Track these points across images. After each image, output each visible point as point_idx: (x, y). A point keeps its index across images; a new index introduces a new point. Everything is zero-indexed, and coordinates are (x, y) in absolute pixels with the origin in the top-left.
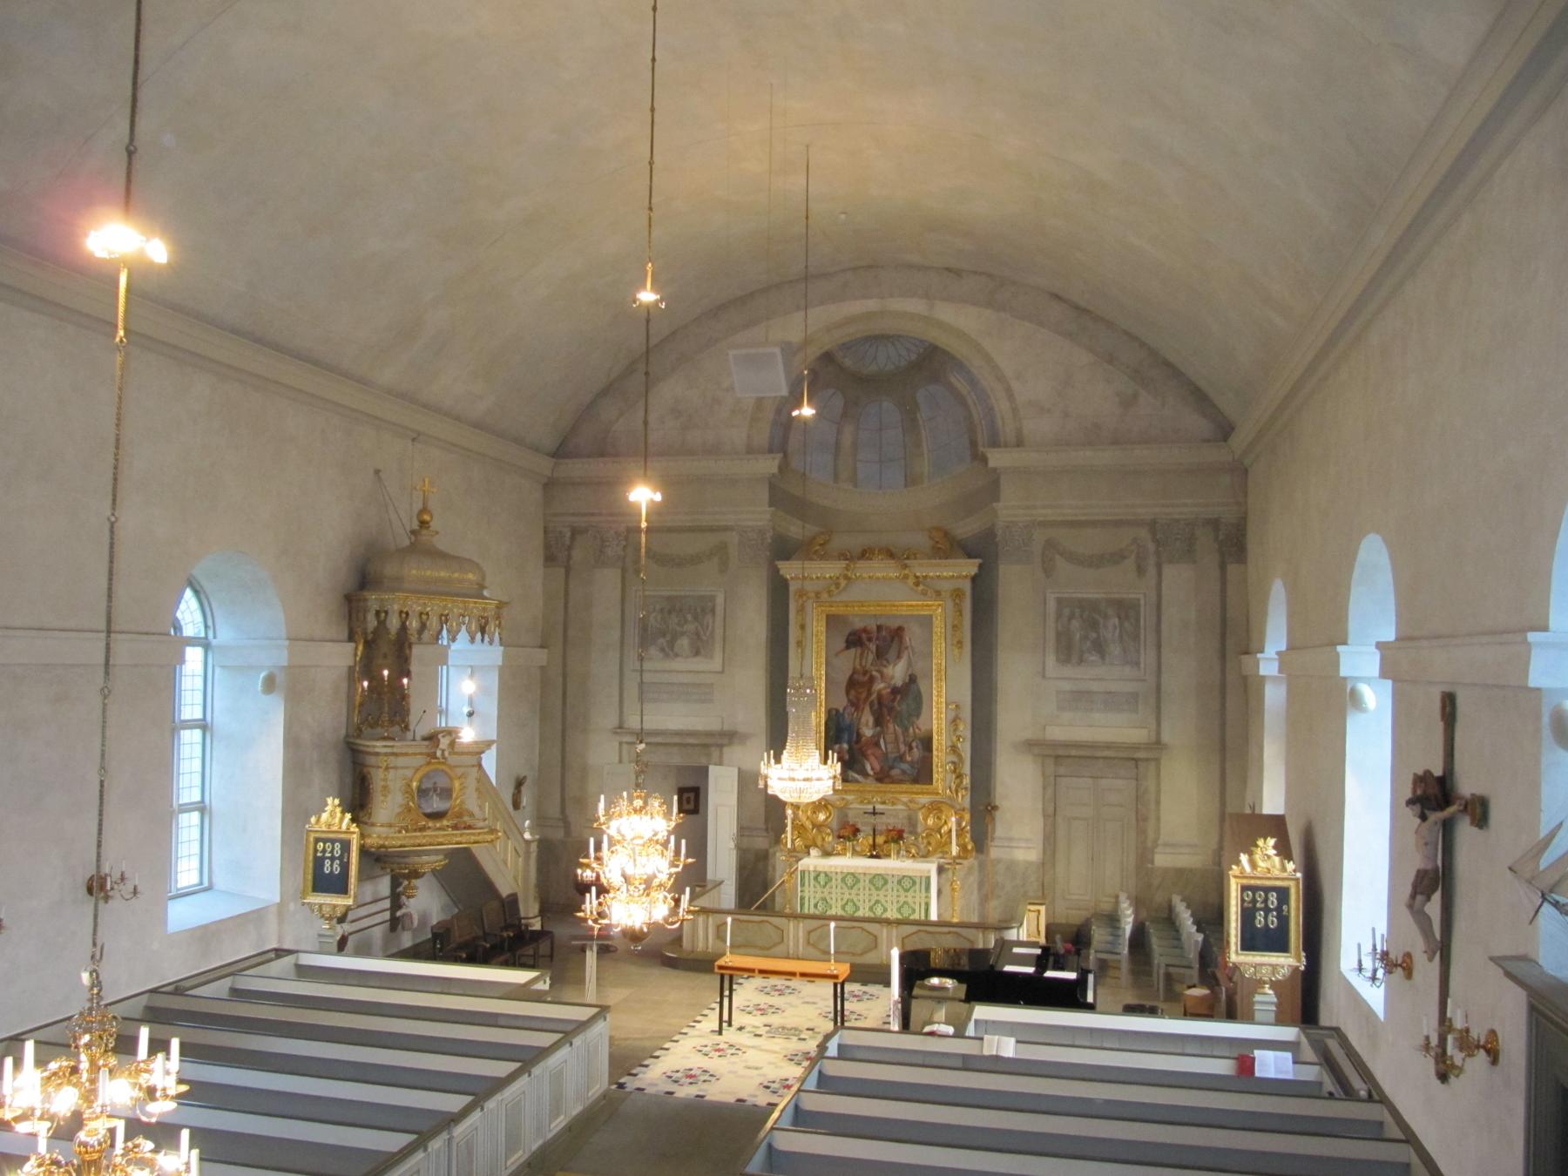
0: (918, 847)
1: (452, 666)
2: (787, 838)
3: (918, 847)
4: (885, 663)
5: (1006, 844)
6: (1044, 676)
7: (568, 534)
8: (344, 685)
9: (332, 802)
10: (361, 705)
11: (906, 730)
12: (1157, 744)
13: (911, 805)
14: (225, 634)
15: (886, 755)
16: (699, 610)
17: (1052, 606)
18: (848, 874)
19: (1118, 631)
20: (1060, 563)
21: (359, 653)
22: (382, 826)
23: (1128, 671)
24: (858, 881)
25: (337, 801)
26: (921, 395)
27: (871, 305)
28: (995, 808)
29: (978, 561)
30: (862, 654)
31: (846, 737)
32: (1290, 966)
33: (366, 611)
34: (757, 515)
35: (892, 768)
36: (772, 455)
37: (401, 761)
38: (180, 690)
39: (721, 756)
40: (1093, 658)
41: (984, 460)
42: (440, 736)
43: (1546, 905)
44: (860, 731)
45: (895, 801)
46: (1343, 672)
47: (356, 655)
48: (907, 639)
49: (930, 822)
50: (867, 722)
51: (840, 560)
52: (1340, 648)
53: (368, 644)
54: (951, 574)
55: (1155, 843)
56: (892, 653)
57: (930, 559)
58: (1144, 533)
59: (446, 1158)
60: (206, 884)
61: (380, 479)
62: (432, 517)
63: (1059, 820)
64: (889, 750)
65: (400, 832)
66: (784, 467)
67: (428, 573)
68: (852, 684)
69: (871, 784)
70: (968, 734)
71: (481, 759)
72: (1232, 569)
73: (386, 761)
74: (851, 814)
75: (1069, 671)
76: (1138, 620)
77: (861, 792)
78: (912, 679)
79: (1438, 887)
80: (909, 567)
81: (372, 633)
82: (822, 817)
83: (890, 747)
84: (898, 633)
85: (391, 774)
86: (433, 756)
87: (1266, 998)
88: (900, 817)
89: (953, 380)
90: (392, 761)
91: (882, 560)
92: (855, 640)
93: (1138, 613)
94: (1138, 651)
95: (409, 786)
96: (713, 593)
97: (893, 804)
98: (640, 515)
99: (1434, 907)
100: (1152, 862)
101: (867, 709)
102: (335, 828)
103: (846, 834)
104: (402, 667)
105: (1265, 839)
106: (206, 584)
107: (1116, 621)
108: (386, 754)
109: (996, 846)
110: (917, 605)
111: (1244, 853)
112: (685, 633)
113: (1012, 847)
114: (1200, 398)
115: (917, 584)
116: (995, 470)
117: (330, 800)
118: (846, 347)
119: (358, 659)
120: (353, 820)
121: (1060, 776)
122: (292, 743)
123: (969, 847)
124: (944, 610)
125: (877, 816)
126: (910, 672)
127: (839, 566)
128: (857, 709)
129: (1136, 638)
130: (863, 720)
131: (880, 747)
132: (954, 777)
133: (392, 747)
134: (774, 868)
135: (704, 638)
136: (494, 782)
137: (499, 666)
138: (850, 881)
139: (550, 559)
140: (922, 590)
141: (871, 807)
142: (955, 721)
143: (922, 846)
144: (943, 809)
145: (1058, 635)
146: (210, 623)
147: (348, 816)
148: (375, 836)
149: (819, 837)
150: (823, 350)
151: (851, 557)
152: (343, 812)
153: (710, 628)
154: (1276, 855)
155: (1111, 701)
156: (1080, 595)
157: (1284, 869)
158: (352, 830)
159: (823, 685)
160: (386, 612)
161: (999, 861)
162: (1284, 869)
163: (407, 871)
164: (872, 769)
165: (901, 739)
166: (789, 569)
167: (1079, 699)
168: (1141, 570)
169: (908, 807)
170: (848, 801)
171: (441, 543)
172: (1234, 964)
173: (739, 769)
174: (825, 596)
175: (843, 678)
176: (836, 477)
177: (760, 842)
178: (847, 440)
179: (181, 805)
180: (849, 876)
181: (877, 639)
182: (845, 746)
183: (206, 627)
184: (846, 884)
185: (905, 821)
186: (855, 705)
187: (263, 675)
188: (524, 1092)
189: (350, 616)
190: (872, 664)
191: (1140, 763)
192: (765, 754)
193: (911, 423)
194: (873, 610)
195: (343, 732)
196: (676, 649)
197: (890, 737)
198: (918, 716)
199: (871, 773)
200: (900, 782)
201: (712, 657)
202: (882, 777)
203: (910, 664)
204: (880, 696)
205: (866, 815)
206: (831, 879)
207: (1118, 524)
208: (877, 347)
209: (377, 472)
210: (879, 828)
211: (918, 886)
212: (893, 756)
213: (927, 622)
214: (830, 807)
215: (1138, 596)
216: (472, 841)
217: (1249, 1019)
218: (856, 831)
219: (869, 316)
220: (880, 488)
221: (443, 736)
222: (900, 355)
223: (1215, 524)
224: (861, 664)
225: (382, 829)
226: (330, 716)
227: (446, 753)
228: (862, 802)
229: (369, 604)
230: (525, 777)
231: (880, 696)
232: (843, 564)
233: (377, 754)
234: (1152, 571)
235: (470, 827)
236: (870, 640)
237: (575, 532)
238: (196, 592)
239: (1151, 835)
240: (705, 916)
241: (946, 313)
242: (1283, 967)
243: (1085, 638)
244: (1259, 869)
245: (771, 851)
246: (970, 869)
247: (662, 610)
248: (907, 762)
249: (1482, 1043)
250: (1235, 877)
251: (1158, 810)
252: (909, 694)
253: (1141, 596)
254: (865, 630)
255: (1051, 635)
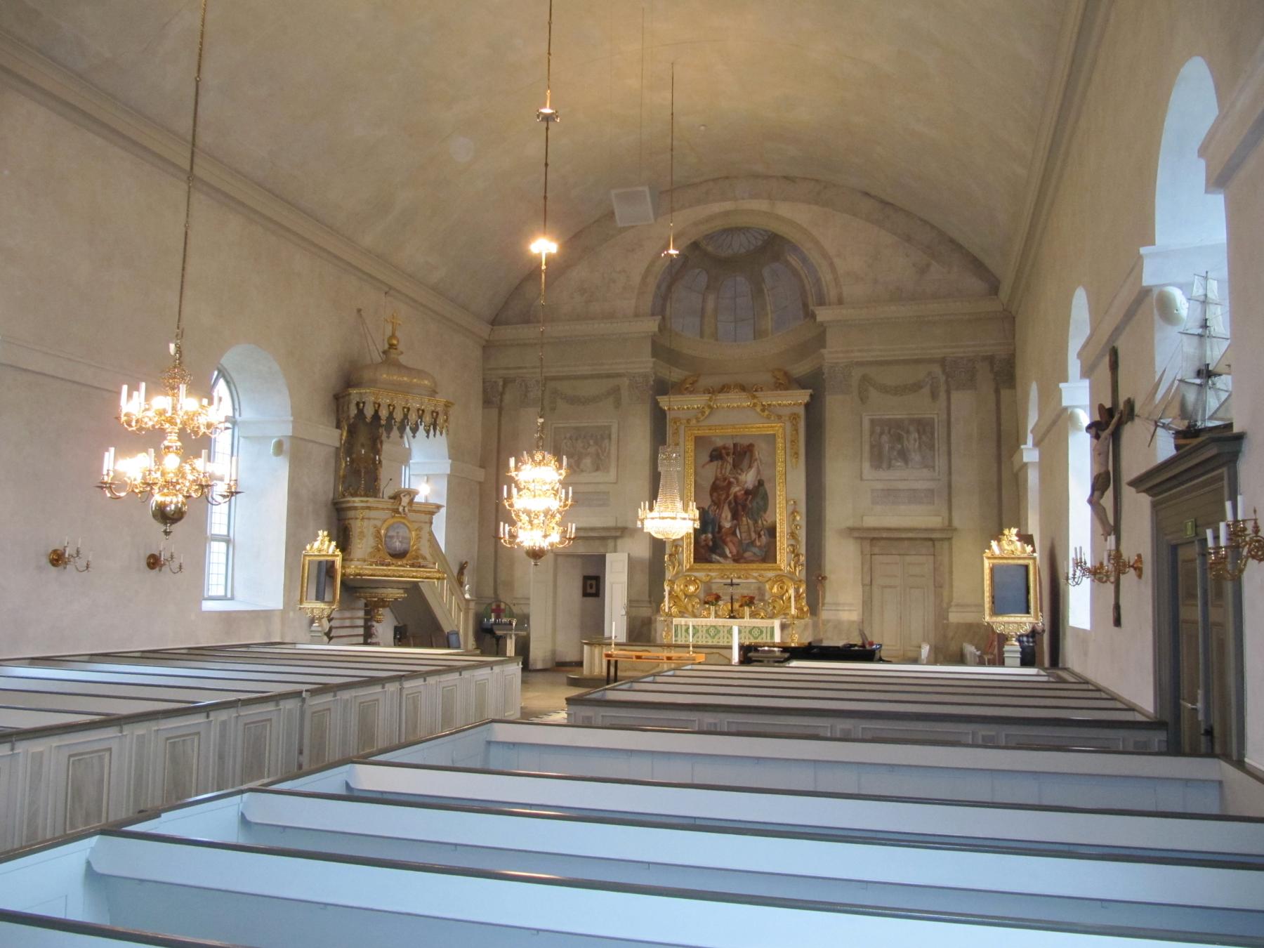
0: (766, 611)
1: (413, 475)
2: (665, 605)
3: (766, 611)
4: (739, 471)
5: (833, 608)
6: (862, 479)
7: (501, 383)
8: (333, 461)
9: (322, 534)
10: (345, 477)
11: (756, 522)
12: (950, 528)
13: (760, 578)
14: (247, 414)
15: (740, 542)
16: (599, 437)
17: (866, 425)
18: (711, 626)
19: (917, 443)
20: (873, 393)
21: (344, 438)
22: (358, 560)
23: (925, 473)
24: (719, 632)
25: (326, 533)
26: (766, 272)
27: (728, 206)
28: (824, 578)
29: (810, 391)
30: (722, 465)
31: (710, 529)
32: (1030, 623)
33: (349, 403)
34: (644, 364)
35: (745, 551)
36: (654, 317)
37: (373, 514)
38: (215, 452)
39: (615, 546)
40: (899, 464)
41: (813, 316)
42: (402, 495)
43: (1158, 429)
44: (721, 524)
45: (748, 576)
46: (1065, 403)
47: (341, 439)
48: (757, 453)
49: (775, 590)
50: (726, 517)
51: (704, 393)
52: (1062, 385)
53: (352, 432)
54: (789, 402)
55: (949, 605)
56: (746, 463)
57: (773, 390)
58: (937, 369)
59: (398, 704)
60: (229, 595)
61: (361, 316)
62: (398, 341)
63: (875, 588)
64: (743, 538)
65: (371, 565)
66: (662, 328)
67: (395, 378)
68: (715, 488)
69: (729, 565)
70: (803, 524)
71: (432, 518)
72: (1005, 393)
73: (362, 513)
74: (714, 587)
75: (883, 474)
76: (933, 434)
77: (723, 570)
78: (761, 483)
79: (1109, 486)
80: (757, 397)
81: (353, 418)
82: (692, 588)
83: (744, 535)
84: (750, 448)
85: (366, 523)
86: (397, 511)
87: (1013, 649)
88: (752, 588)
89: (789, 258)
90: (367, 513)
91: (737, 392)
92: (717, 455)
93: (933, 427)
94: (933, 457)
95: (379, 532)
96: (610, 424)
97: (747, 578)
98: (541, 262)
99: (1107, 500)
100: (947, 619)
101: (726, 507)
102: (324, 553)
103: (710, 599)
104: (375, 445)
105: (1010, 529)
106: (234, 375)
107: (917, 435)
108: (363, 508)
109: (827, 610)
110: (763, 427)
111: (994, 540)
112: (589, 454)
113: (838, 610)
114: (977, 266)
115: (763, 410)
116: (822, 324)
117: (320, 533)
118: (710, 237)
119: (343, 442)
120: (337, 547)
121: (874, 554)
122: (293, 494)
123: (805, 609)
124: (784, 429)
125: (735, 587)
126: (759, 478)
127: (704, 398)
128: (718, 507)
129: (932, 447)
130: (723, 515)
131: (737, 537)
132: (793, 556)
133: (367, 502)
134: (656, 630)
135: (603, 458)
136: (444, 551)
137: (448, 475)
138: (712, 632)
139: (487, 402)
140: (767, 415)
141: (729, 581)
142: (793, 513)
143: (769, 610)
144: (784, 580)
145: (872, 447)
146: (237, 407)
147: (334, 543)
148: (353, 567)
149: (690, 605)
150: (693, 240)
151: (714, 391)
152: (330, 541)
153: (607, 450)
154: (1018, 540)
155: (914, 497)
156: (887, 417)
157: (1024, 551)
158: (336, 553)
159: (693, 490)
160: (364, 403)
161: (828, 621)
162: (1024, 551)
163: (376, 599)
164: (731, 552)
165: (753, 529)
166: (664, 402)
167: (889, 496)
168: (934, 395)
169: (758, 580)
170: (711, 577)
171: (403, 359)
172: (988, 623)
173: (629, 555)
174: (694, 422)
175: (707, 485)
176: (702, 336)
177: (645, 612)
178: (710, 305)
179: (212, 535)
180: (711, 629)
181: (734, 454)
182: (710, 536)
183: (234, 409)
184: (710, 635)
185: (756, 592)
186: (717, 504)
187: (274, 441)
188: (456, 685)
189: (338, 411)
190: (730, 473)
191: (936, 543)
192: (642, 503)
193: (758, 292)
194: (730, 431)
195: (331, 496)
196: (582, 466)
197: (744, 528)
198: (765, 511)
199: (729, 555)
200: (752, 562)
201: (608, 472)
202: (737, 559)
203: (758, 472)
204: (736, 497)
205: (726, 586)
206: (698, 631)
207: (917, 362)
208: (732, 237)
209: (359, 311)
210: (735, 597)
211: (764, 635)
212: (747, 542)
213: (771, 439)
214: (698, 581)
215: (932, 416)
216: (425, 576)
217: (1002, 663)
218: (718, 598)
219: (727, 214)
220: (735, 341)
221: (404, 496)
222: (749, 242)
223: (990, 359)
224: (721, 473)
225: (358, 563)
226: (322, 482)
227: (406, 509)
228: (722, 577)
229: (352, 397)
230: (466, 563)
231: (736, 497)
232: (707, 397)
233: (355, 508)
234: (943, 395)
235: (423, 567)
236: (728, 454)
237: (506, 382)
238: (228, 382)
239: (946, 600)
240: (600, 648)
241: (784, 209)
242: (1025, 624)
243: (892, 448)
244: (1005, 552)
245: (653, 618)
246: (806, 626)
247: (571, 438)
248: (756, 546)
249: (1131, 564)
250: (988, 558)
251: (951, 580)
252: (758, 496)
253: (935, 416)
254: (724, 448)
255: (867, 448)
